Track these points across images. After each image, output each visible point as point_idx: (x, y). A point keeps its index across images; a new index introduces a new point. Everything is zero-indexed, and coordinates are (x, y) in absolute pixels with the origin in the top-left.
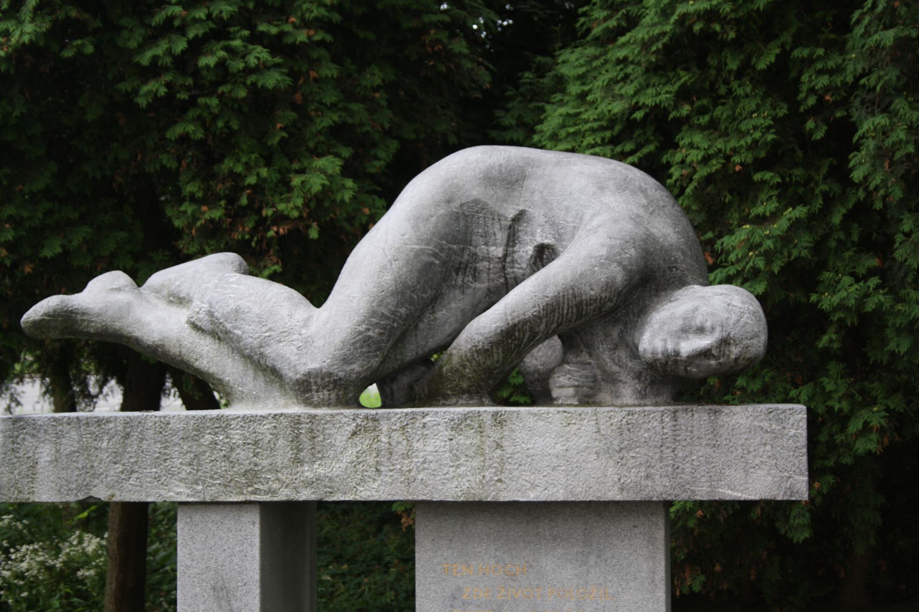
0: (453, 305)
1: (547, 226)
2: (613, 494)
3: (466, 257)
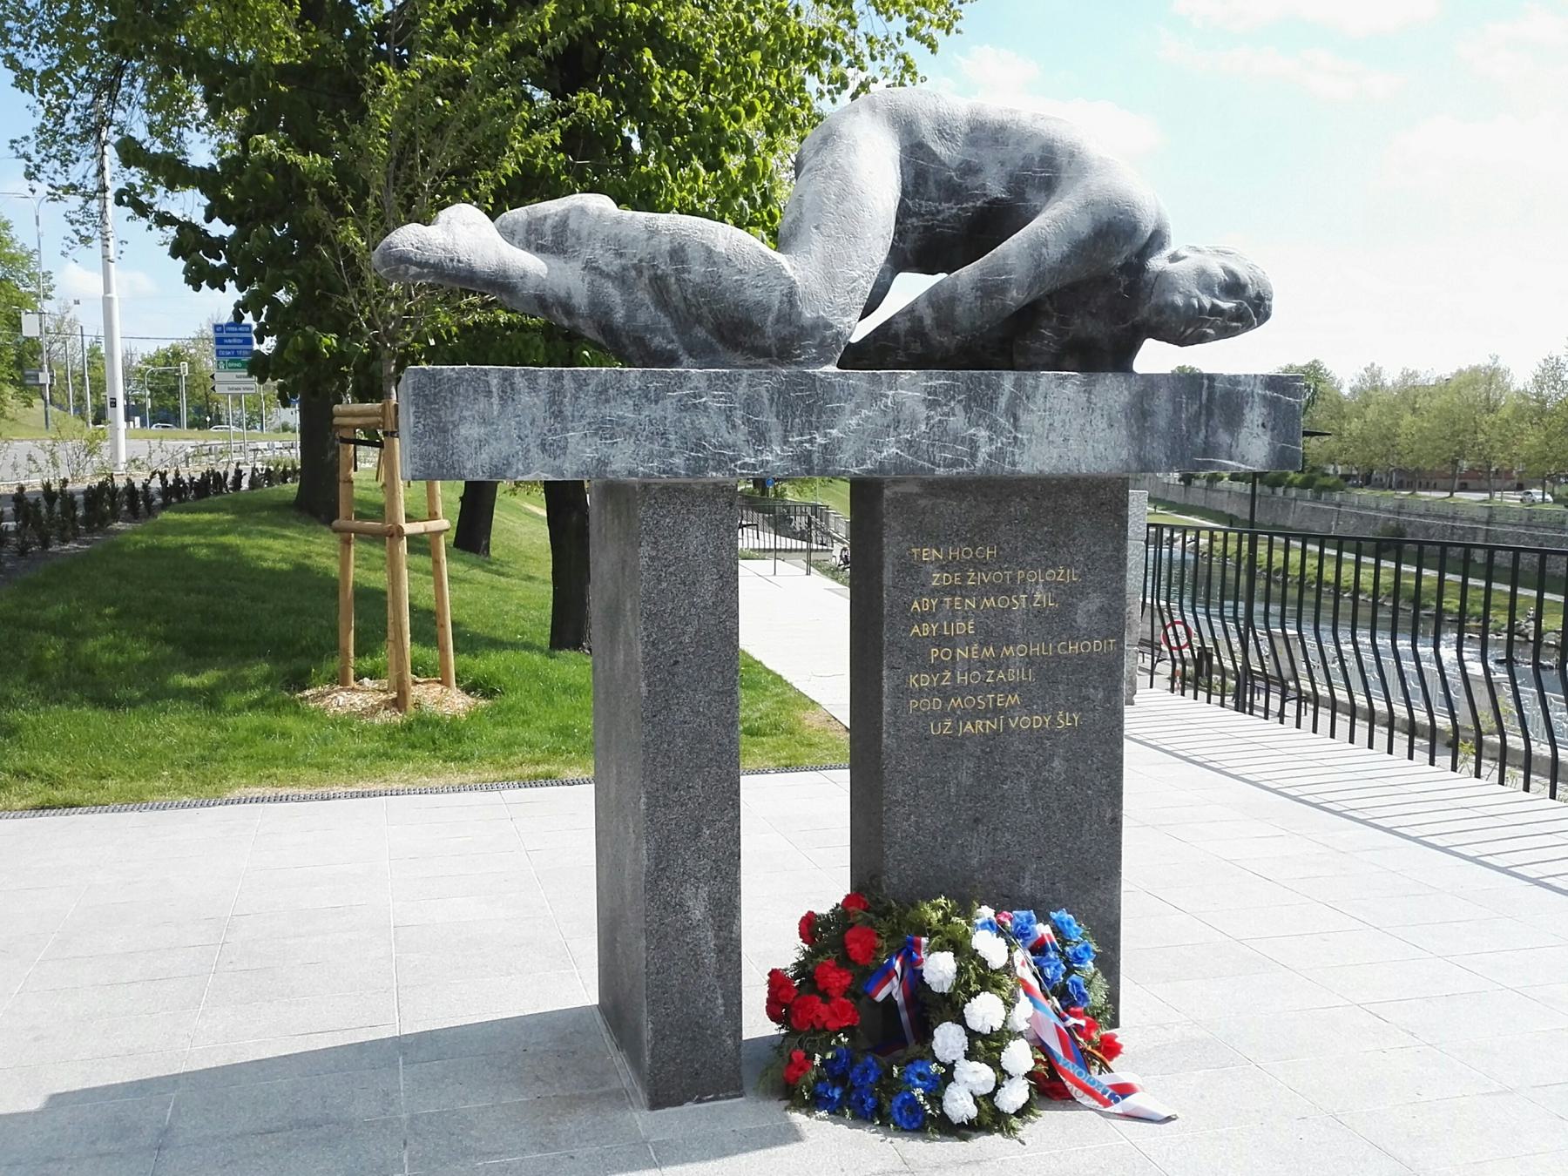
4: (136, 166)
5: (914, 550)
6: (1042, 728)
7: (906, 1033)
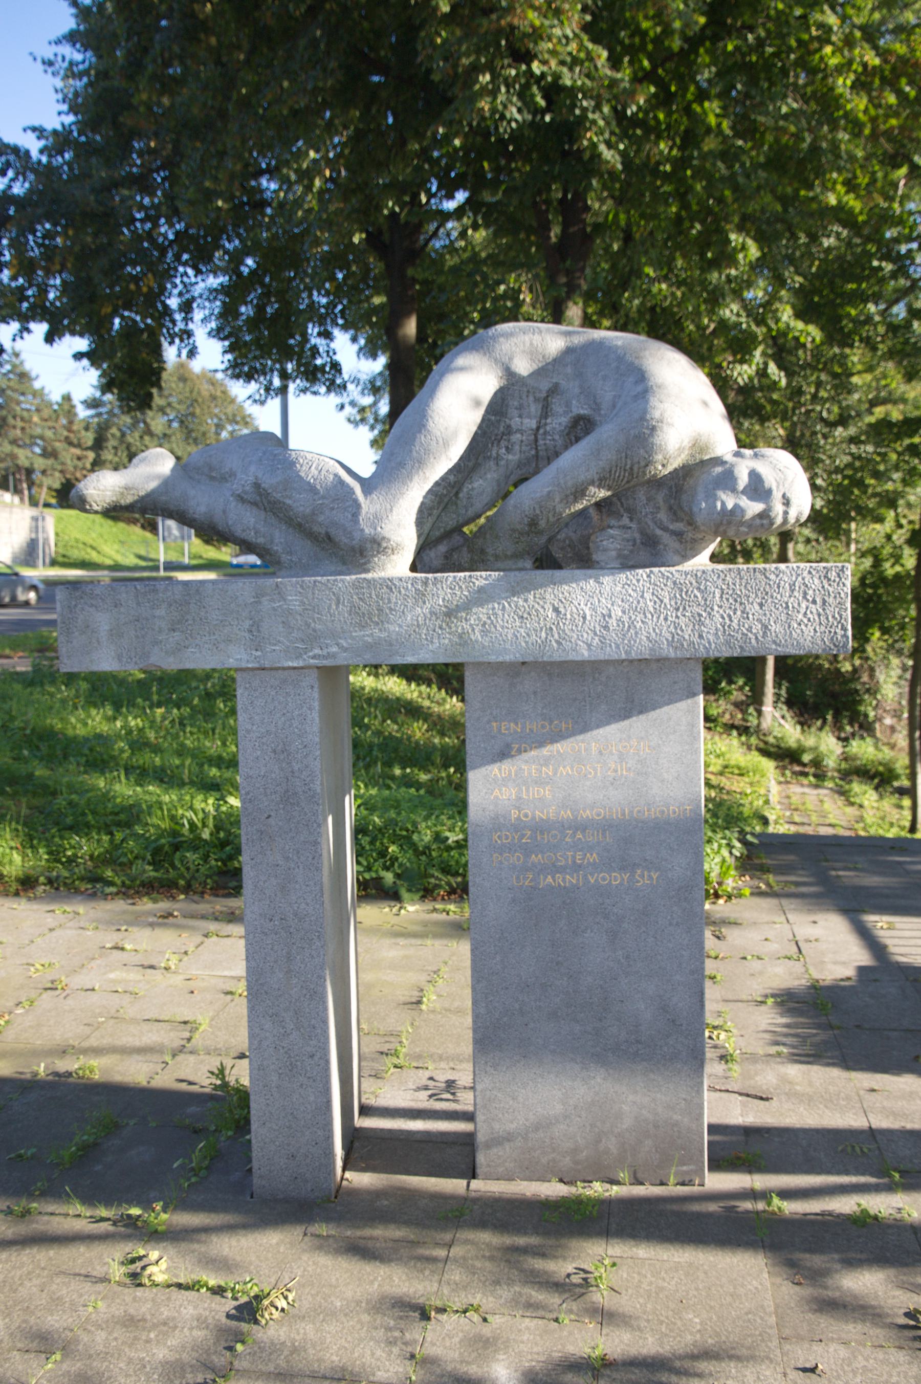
0: (489, 476)
1: (582, 397)
2: (214, 1238)
3: (502, 429)
5: (494, 724)
6: (621, 884)
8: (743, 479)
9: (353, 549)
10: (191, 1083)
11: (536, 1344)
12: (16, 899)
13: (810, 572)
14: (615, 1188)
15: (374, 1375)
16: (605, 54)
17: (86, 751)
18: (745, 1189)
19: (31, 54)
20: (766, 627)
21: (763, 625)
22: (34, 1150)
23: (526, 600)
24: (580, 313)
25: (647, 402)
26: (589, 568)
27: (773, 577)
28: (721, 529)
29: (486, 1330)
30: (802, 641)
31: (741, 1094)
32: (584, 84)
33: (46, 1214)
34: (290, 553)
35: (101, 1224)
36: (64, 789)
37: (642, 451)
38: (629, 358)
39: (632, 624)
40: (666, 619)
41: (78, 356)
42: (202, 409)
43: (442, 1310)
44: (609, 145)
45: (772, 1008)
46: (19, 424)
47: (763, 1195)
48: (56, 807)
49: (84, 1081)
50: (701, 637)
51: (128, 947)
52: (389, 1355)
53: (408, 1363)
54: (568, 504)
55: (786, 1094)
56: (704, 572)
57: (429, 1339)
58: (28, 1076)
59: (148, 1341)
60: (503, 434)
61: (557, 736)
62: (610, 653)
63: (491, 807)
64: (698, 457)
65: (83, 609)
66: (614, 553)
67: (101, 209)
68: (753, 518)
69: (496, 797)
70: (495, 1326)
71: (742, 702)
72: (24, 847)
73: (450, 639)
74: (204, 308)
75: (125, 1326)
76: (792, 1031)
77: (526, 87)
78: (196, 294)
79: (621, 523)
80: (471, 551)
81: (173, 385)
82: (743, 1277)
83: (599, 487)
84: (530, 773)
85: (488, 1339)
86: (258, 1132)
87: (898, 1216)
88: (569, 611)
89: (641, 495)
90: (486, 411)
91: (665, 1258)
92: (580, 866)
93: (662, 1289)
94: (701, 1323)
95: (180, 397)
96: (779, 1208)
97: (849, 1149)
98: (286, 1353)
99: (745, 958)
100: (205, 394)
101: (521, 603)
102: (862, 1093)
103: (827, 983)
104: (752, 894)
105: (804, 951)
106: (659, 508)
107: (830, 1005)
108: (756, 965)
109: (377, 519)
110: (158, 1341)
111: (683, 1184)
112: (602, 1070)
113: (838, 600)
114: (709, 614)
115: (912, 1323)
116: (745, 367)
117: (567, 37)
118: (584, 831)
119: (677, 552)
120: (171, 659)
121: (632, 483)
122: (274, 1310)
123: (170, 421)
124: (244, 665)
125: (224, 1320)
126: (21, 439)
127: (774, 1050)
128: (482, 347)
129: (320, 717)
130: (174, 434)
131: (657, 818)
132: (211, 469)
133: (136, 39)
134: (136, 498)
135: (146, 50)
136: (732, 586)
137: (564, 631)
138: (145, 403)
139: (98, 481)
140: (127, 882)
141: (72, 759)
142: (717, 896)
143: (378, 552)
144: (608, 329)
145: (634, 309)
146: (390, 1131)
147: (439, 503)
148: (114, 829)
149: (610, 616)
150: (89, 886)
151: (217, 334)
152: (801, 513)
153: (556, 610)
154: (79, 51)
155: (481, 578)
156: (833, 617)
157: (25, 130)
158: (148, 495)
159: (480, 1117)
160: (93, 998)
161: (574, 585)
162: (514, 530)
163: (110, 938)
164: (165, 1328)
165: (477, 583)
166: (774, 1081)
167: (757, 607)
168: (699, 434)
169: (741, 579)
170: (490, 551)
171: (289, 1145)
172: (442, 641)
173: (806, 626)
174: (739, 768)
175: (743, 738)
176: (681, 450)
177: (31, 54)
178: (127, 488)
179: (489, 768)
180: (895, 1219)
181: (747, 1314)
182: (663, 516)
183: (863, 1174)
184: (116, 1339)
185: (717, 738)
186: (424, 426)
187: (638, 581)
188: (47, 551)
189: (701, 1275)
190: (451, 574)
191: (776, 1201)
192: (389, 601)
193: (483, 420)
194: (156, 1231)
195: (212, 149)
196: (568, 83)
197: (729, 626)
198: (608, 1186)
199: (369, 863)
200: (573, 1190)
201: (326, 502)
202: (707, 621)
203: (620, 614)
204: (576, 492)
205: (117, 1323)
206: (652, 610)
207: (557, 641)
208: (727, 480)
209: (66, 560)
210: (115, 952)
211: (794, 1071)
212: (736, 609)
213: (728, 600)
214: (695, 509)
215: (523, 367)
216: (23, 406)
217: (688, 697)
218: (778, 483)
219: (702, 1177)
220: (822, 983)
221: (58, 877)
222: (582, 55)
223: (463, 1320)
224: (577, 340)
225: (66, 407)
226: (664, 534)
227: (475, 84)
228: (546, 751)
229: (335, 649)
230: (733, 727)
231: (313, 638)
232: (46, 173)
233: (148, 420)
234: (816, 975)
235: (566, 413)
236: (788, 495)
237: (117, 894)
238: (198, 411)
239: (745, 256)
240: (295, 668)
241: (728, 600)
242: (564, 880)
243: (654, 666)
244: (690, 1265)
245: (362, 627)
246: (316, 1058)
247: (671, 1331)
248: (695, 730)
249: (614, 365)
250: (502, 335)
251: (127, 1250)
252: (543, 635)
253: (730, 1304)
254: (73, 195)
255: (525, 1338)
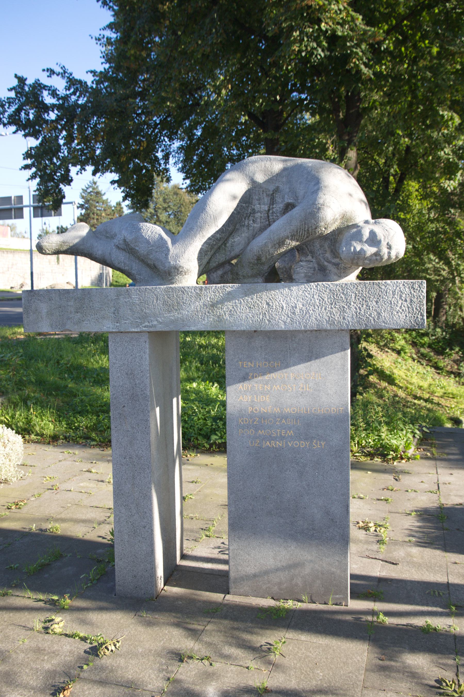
0: (243, 235)
3: (250, 211)
4: (436, 296)
6: (305, 447)
7: (207, 593)
8: (366, 234)
9: (165, 272)
10: (104, 538)
11: (234, 679)
12: (48, 446)
13: (403, 285)
14: (299, 604)
15: (147, 686)
16: (361, 17)
17: (95, 376)
18: (369, 609)
19: (90, 35)
20: (379, 314)
21: (377, 313)
22: (18, 565)
23: (252, 299)
24: (355, 155)
25: (317, 195)
26: (292, 282)
27: (383, 287)
28: (355, 262)
29: (210, 669)
30: (399, 321)
31: (382, 561)
32: (348, 33)
33: (15, 596)
34: (140, 275)
35: (39, 603)
36: (80, 394)
37: (313, 221)
38: (313, 172)
39: (307, 312)
40: (325, 309)
41: (113, 182)
42: (185, 209)
43: (191, 658)
44: (366, 65)
45: (414, 517)
46: (96, 217)
47: (373, 613)
48: (74, 402)
49: (53, 534)
50: (344, 318)
51: (93, 471)
52: (157, 677)
53: (165, 682)
54: (276, 249)
55: (407, 562)
56: (346, 284)
57: (180, 671)
58: (27, 530)
59: (43, 660)
60: (251, 213)
61: (273, 370)
62: (296, 327)
63: (238, 406)
64: (346, 224)
65: (34, 302)
66: (303, 275)
67: (120, 109)
68: (372, 255)
69: (241, 400)
70: (215, 668)
71: (458, 360)
72: (56, 421)
73: (213, 319)
74: (175, 157)
75: (35, 652)
76: (421, 530)
77: (318, 36)
78: (172, 150)
79: (307, 259)
80: (232, 274)
81: (171, 197)
82: (353, 654)
83: (292, 240)
84: (258, 389)
85: (210, 674)
86: (119, 563)
87: (448, 629)
88: (275, 304)
89: (317, 244)
90: (240, 201)
91: (315, 641)
92: (284, 437)
93: (308, 656)
94: (323, 676)
95: (174, 202)
96: (383, 620)
97: (432, 592)
98: (107, 672)
99: (407, 491)
100: (187, 201)
101: (250, 300)
102: (449, 564)
103: (448, 506)
104: (421, 458)
105: (440, 489)
106: (326, 251)
107: (446, 518)
108: (413, 495)
109: (177, 256)
110: (48, 661)
111: (336, 604)
112: (295, 543)
113: (419, 299)
114: (349, 307)
115: (438, 685)
116: (452, 182)
117: (340, 10)
118: (286, 419)
119: (336, 274)
120: (76, 327)
121: (310, 238)
122: (106, 651)
123: (170, 215)
124: (111, 330)
125: (82, 653)
126: (96, 224)
127: (407, 539)
128: (240, 169)
129: (150, 357)
130: (171, 221)
131: (324, 414)
132: (107, 232)
133: (128, 24)
134: (68, 247)
135: (133, 29)
136: (361, 292)
137: (272, 315)
138: (146, 206)
139: (49, 239)
140: (102, 440)
141: (87, 379)
142: (402, 458)
143: (178, 274)
144: (263, 154)
145: (390, 153)
146: (194, 568)
147: (211, 249)
148: (100, 413)
149: (296, 307)
150: (84, 441)
151: (179, 170)
152: (398, 253)
153: (268, 304)
154: (114, 33)
155: (229, 287)
156: (416, 309)
157: (87, 72)
158: (74, 246)
159: (231, 563)
160: (69, 494)
161: (277, 291)
162: (250, 263)
163: (86, 466)
164: (53, 655)
165: (227, 290)
166: (403, 555)
167: (375, 303)
168: (345, 212)
169: (366, 288)
170: (240, 273)
171: (133, 571)
172: (209, 319)
173: (401, 313)
174: (453, 394)
175: (457, 379)
176: (335, 220)
177: (90, 35)
178: (64, 242)
179: (238, 385)
180: (446, 631)
181: (349, 673)
182: (328, 255)
183: (436, 606)
184: (28, 658)
185: (442, 378)
186: (205, 209)
187: (311, 289)
188: (108, 279)
189: (331, 651)
190: (214, 285)
191: (381, 616)
192: (183, 298)
193: (238, 206)
194: (63, 608)
195: (166, 77)
196: (340, 34)
197: (359, 313)
198: (296, 602)
199: (221, 434)
200: (278, 603)
201: (154, 248)
202: (348, 310)
203: (301, 306)
204: (279, 242)
205: (31, 650)
206: (318, 304)
207: (268, 320)
208: (358, 236)
209: (117, 284)
210: (87, 473)
211: (415, 551)
212: (363, 304)
213: (359, 299)
214: (340, 251)
215: (260, 178)
216: (98, 208)
217: (341, 351)
218: (385, 237)
219: (347, 602)
220: (445, 506)
221: (69, 436)
222: (349, 19)
223: (200, 663)
224: (290, 164)
225: (118, 209)
226: (329, 265)
227: (291, 37)
228: (266, 377)
229: (155, 323)
230: (452, 372)
231: (145, 317)
232: (95, 92)
233: (159, 214)
234: (443, 501)
235: (282, 202)
236: (390, 243)
237: (96, 445)
238: (183, 210)
239: (453, 123)
240: (137, 332)
241: (359, 299)
242: (275, 444)
243: (324, 334)
244: (327, 645)
245: (169, 312)
246: (146, 528)
247: (306, 678)
248: (346, 368)
249: (305, 176)
250: (250, 162)
251: (47, 616)
252: (261, 317)
253: (342, 668)
254: (106, 103)
255: (229, 675)
